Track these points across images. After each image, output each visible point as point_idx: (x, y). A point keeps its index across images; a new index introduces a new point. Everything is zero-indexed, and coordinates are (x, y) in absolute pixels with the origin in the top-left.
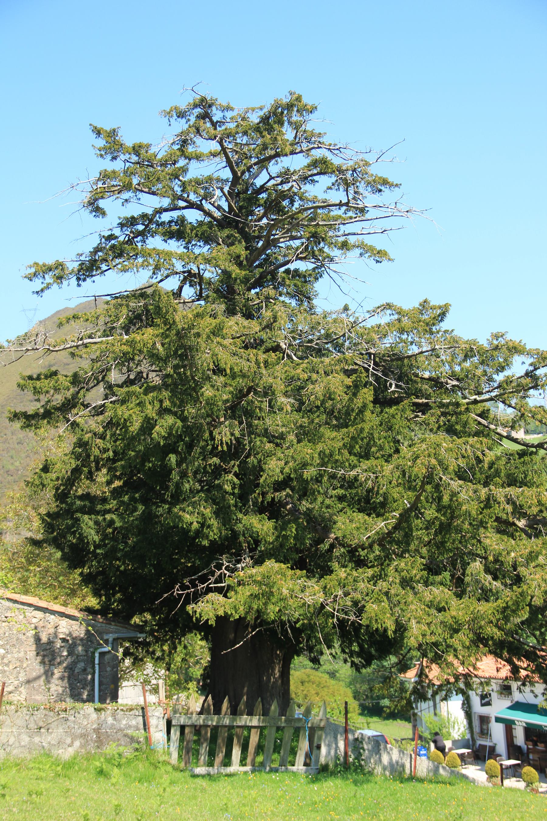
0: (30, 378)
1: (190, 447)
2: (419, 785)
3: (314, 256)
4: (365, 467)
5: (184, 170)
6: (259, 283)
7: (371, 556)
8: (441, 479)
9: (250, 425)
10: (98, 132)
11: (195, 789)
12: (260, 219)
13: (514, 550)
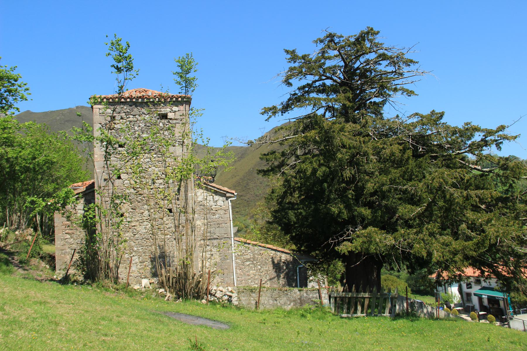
0: (265, 155)
1: (333, 179)
2: (441, 322)
3: (382, 95)
4: (410, 185)
5: (324, 64)
6: (358, 109)
7: (415, 223)
8: (445, 188)
9: (358, 169)
10: (287, 52)
11: (343, 323)
12: (357, 81)
13: (481, 218)
